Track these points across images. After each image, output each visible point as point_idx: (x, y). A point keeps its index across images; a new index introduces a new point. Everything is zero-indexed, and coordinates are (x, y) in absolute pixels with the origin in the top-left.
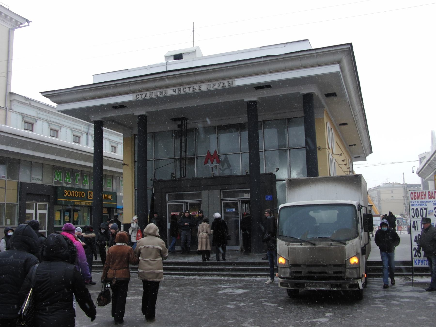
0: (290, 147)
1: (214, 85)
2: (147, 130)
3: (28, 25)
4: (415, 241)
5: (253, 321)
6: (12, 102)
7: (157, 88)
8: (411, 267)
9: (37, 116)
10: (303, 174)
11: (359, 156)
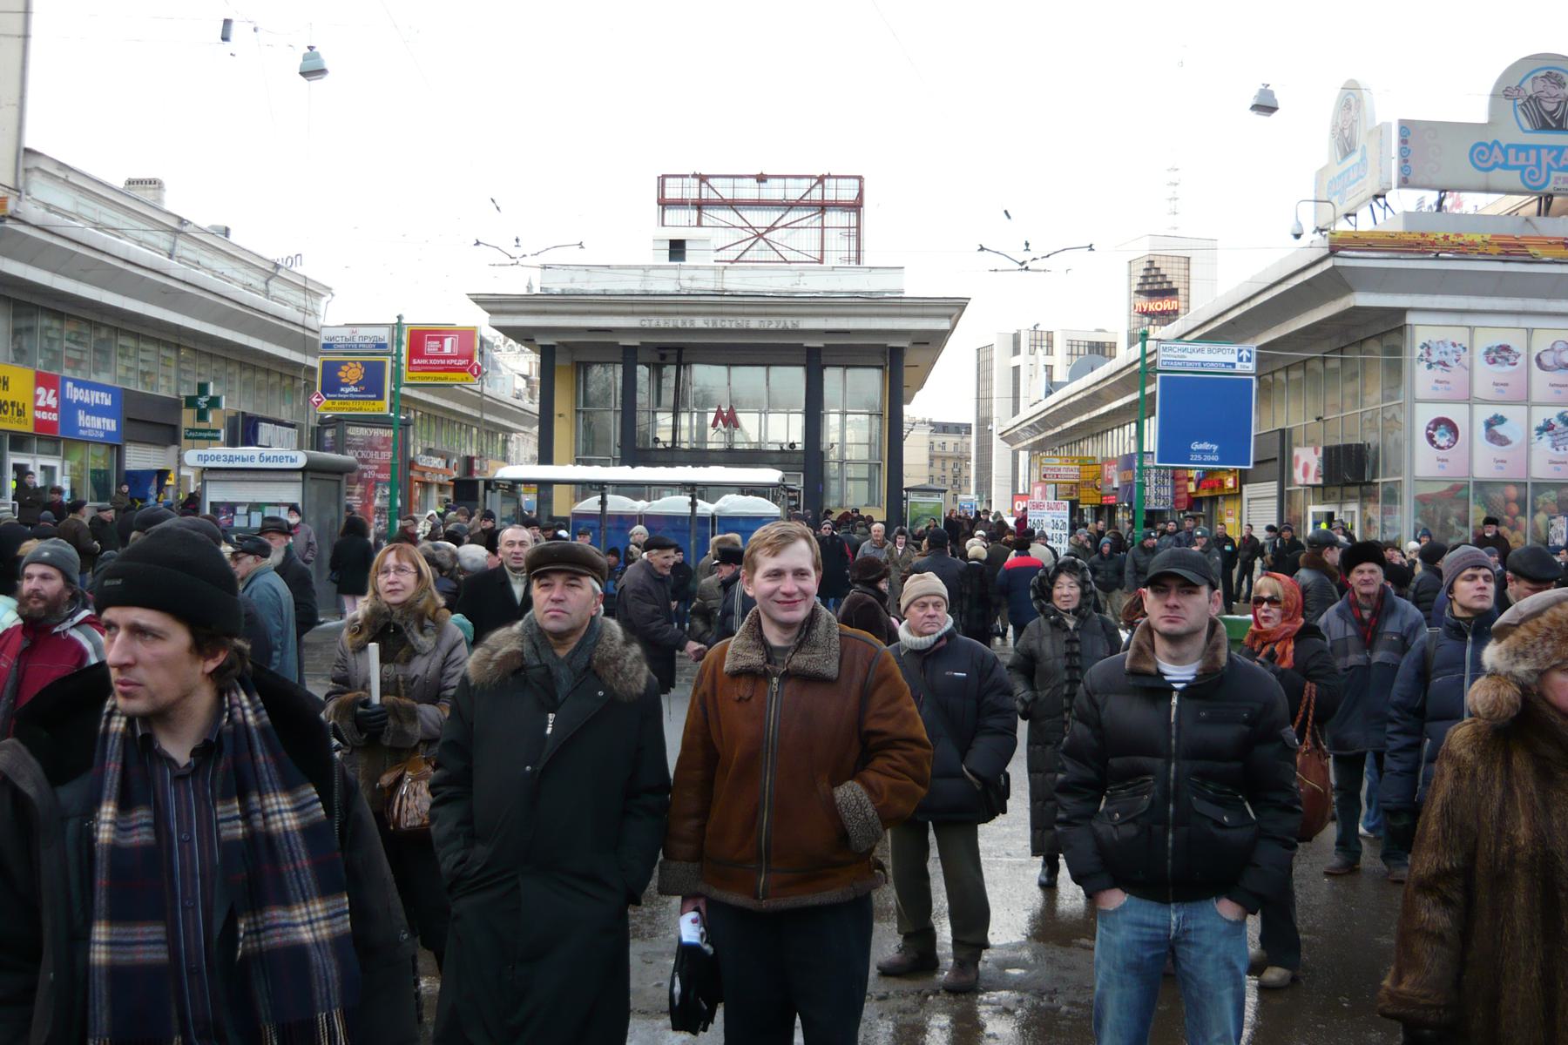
0: (334, 485)
1: (770, 323)
5: (1024, 718)
6: (29, 175)
9: (74, 211)
10: (1483, 705)
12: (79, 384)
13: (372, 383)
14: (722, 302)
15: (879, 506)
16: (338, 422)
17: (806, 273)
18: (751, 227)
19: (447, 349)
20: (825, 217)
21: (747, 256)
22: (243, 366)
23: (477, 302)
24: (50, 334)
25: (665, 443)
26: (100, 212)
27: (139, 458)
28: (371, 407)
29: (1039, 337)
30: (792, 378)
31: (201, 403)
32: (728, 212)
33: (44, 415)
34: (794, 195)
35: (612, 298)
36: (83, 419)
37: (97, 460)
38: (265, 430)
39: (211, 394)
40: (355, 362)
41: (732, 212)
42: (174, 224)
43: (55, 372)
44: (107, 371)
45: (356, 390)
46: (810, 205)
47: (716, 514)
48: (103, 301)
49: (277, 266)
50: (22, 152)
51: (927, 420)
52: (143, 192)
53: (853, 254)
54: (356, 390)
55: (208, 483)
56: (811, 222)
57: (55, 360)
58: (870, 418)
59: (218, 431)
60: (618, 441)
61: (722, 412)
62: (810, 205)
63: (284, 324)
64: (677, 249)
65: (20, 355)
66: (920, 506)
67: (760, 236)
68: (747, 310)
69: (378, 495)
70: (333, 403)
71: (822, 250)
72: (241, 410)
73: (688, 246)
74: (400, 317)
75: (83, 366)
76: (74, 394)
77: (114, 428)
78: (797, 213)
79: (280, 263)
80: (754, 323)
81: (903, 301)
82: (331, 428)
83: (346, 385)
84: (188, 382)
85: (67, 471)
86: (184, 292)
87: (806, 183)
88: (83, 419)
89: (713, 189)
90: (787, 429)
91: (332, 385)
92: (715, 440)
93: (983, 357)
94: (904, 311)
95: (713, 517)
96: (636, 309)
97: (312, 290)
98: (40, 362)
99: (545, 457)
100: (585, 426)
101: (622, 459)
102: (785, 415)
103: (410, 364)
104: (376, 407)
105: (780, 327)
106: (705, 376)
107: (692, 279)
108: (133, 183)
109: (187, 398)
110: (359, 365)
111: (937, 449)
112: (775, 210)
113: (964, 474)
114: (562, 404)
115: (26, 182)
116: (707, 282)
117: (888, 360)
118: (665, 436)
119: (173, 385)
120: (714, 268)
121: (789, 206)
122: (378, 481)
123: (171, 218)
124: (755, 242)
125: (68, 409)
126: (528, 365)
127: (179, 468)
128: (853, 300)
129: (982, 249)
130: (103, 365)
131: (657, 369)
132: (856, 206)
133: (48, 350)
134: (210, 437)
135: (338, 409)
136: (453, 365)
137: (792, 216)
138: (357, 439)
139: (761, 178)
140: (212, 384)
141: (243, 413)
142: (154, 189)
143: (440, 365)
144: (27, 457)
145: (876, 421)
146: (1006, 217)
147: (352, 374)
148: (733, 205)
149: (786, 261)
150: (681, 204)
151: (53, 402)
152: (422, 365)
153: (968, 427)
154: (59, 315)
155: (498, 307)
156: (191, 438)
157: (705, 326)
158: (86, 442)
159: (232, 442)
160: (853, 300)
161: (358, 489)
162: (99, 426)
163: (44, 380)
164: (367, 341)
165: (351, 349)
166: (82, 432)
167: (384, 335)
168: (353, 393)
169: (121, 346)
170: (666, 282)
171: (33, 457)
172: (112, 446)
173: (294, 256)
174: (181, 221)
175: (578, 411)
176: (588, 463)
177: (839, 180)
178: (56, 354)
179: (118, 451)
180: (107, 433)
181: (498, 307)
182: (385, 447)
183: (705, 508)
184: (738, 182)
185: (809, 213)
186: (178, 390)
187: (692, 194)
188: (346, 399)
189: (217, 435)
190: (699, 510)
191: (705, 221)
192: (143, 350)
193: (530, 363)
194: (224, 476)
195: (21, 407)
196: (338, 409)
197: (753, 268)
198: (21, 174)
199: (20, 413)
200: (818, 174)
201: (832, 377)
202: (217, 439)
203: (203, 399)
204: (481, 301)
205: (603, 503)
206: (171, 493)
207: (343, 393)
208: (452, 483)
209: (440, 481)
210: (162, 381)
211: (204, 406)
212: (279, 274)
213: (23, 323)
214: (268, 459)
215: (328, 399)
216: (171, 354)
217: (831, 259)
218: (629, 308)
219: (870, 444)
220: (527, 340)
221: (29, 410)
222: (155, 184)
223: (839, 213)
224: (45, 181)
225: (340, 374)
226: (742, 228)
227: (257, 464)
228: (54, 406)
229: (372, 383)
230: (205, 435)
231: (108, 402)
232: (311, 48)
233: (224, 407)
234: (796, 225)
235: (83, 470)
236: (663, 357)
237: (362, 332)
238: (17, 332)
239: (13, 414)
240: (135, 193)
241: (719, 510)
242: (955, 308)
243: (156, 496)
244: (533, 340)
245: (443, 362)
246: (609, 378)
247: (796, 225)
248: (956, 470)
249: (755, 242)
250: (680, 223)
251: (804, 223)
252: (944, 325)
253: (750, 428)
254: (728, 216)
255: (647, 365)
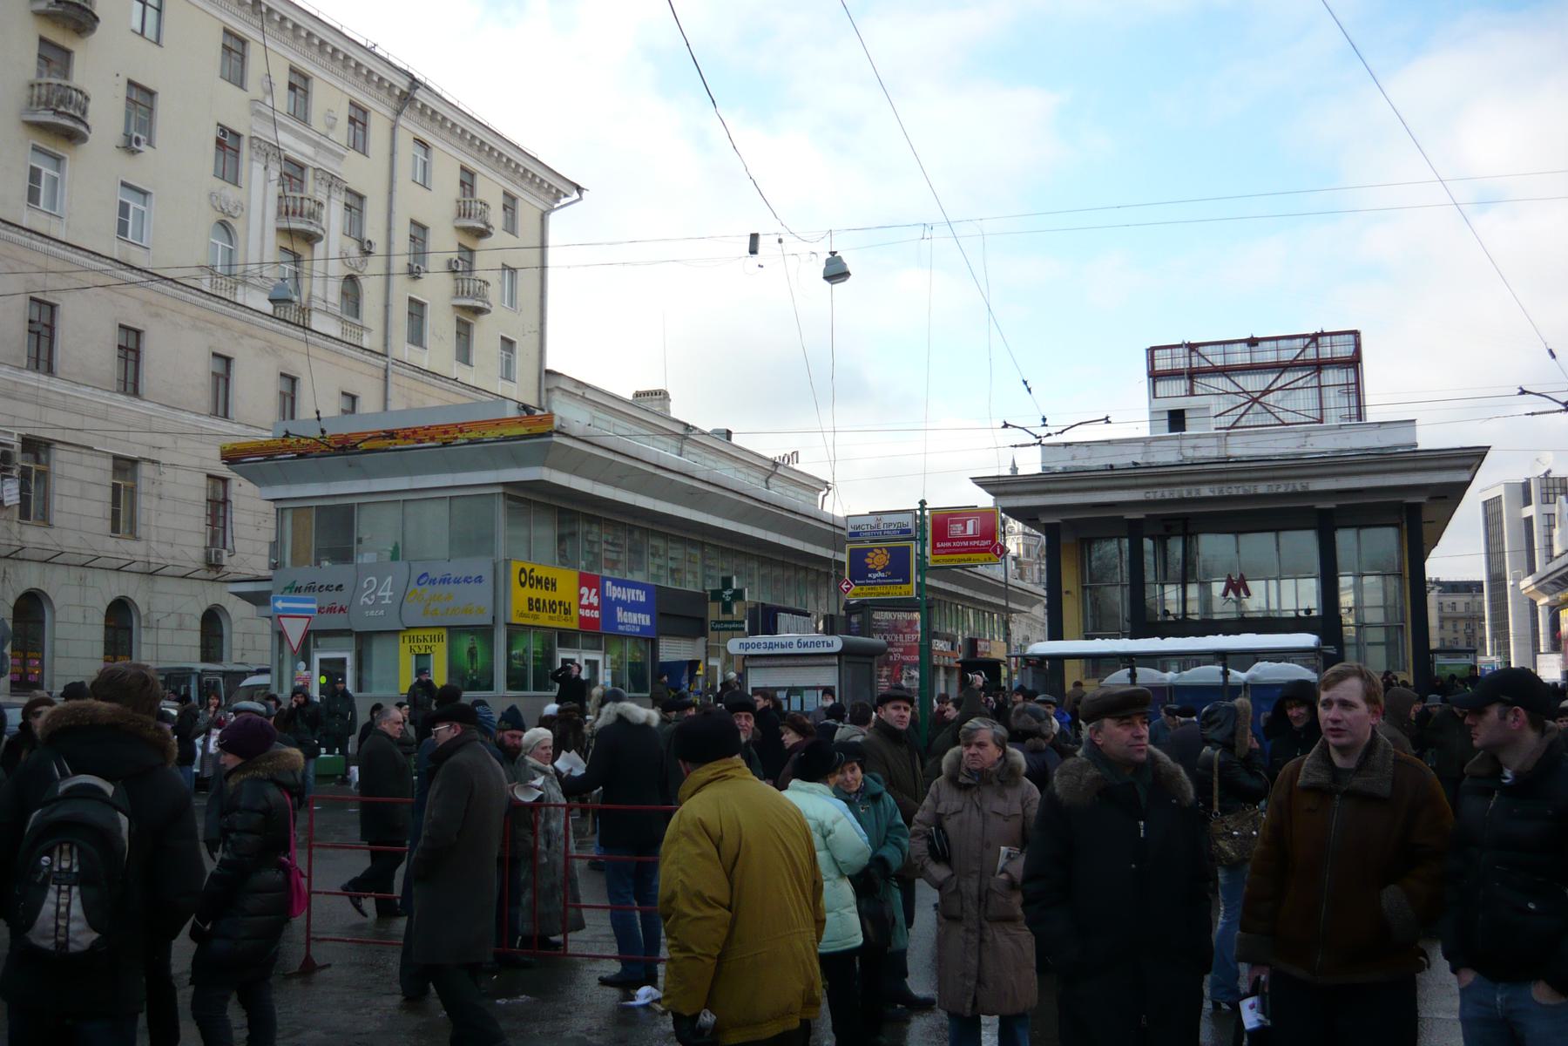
1: (1279, 487)
2: (1431, 644)
3: (581, 199)
4: (844, 609)
6: (550, 394)
7: (1182, 484)
8: (407, 853)
11: (1219, 431)
12: (616, 583)
13: (898, 567)
14: (1226, 469)
15: (1404, 670)
16: (863, 607)
17: (1313, 433)
18: (1245, 392)
19: (970, 531)
20: (1322, 375)
21: (1243, 422)
22: (764, 561)
23: (977, 483)
24: (590, 537)
25: (1175, 616)
26: (614, 424)
27: (673, 650)
28: (898, 591)
29: (1551, 484)
30: (1305, 542)
31: (725, 596)
32: (1220, 379)
33: (587, 613)
34: (1287, 356)
35: (1160, 470)
36: (622, 616)
37: (630, 652)
38: (784, 618)
39: (735, 587)
40: (880, 548)
41: (1224, 379)
42: (680, 430)
43: (596, 573)
44: (640, 570)
45: (883, 575)
46: (1305, 365)
47: (1250, 682)
48: (637, 505)
49: (775, 464)
50: (544, 373)
51: (1433, 579)
52: (649, 403)
53: (1354, 411)
54: (883, 575)
55: (749, 670)
56: (1307, 382)
57: (596, 560)
58: (1385, 581)
59: (743, 623)
60: (1126, 615)
61: (1233, 581)
62: (1305, 365)
63: (798, 518)
64: (1177, 419)
65: (565, 560)
66: (1448, 668)
67: (1255, 400)
68: (1276, 474)
69: (904, 676)
70: (862, 589)
71: (1321, 409)
72: (760, 602)
73: (1187, 415)
74: (923, 503)
75: (620, 566)
76: (614, 592)
77: (648, 623)
78: (1291, 374)
79: (777, 460)
80: (1262, 488)
81: (1418, 454)
82: (858, 613)
83: (875, 571)
84: (710, 577)
85: (608, 665)
86: (708, 492)
87: (1299, 343)
88: (622, 616)
89: (1203, 356)
90: (1302, 595)
91: (860, 571)
92: (1222, 608)
93: (1491, 510)
94: (1419, 465)
95: (1246, 684)
96: (1140, 481)
97: (818, 486)
98: (583, 563)
99: (1056, 633)
100: (1092, 603)
101: (1131, 633)
102: (1293, 581)
103: (934, 547)
104: (902, 591)
105: (1289, 490)
106: (1214, 547)
107: (1194, 447)
108: (640, 396)
109: (712, 591)
110: (885, 551)
111: (1447, 610)
112: (1268, 373)
113: (1478, 634)
114: (1069, 582)
115: (549, 401)
116: (1210, 451)
117: (1405, 517)
118: (1174, 608)
119: (699, 580)
120: (1216, 436)
121: (1280, 367)
122: (904, 663)
123: (677, 424)
124: (1250, 407)
125: (607, 606)
126: (1016, 546)
127: (707, 659)
128: (1365, 458)
129: (1006, 426)
130: (636, 563)
131: (1161, 541)
132: (1353, 362)
133: (588, 552)
134: (735, 628)
135: (866, 594)
136: (976, 546)
137: (1287, 377)
138: (883, 624)
139: (1253, 342)
140: (734, 578)
141: (763, 604)
142: (660, 399)
143: (963, 547)
144: (573, 652)
145: (1393, 583)
146: (1549, 357)
147: (878, 560)
148: (1225, 371)
149: (1284, 424)
150: (1173, 374)
151: (595, 601)
152: (946, 548)
153: (1480, 584)
154: (592, 519)
155: (1002, 489)
156: (717, 630)
157: (1211, 494)
158: (623, 637)
159: (754, 631)
160: (1365, 458)
161: (885, 672)
162: (635, 621)
163: (587, 580)
164: (892, 528)
165: (877, 536)
166: (621, 628)
167: (908, 521)
168: (881, 578)
169: (653, 547)
170: (1166, 455)
171: (578, 653)
172: (646, 640)
173: (790, 454)
174: (687, 426)
175: (1084, 588)
176: (1092, 638)
177: (1334, 337)
178: (597, 556)
179: (654, 645)
180: (642, 627)
181: (1002, 489)
182: (909, 630)
183: (1237, 676)
184: (1229, 348)
185: (1304, 374)
186: (704, 585)
187: (1181, 363)
188: (875, 584)
189: (742, 626)
190: (1231, 679)
191: (1198, 390)
192: (671, 548)
193: (1018, 544)
194: (764, 662)
195: (567, 606)
196: (866, 594)
197: (1257, 433)
198: (544, 393)
199: (567, 611)
200: (1311, 331)
201: (1345, 539)
202: (743, 629)
203: (728, 592)
204: (984, 483)
205: (1133, 676)
206: (700, 682)
207: (871, 579)
208: (959, 665)
209: (947, 664)
210: (689, 577)
211: (728, 599)
212: (778, 471)
213: (566, 531)
214: (806, 645)
215: (856, 585)
216: (697, 553)
217: (1332, 419)
218: (1133, 482)
219: (1385, 607)
220: (1030, 520)
221: (574, 608)
222: (662, 395)
223: (1336, 371)
224: (565, 400)
225: (867, 561)
226: (1236, 393)
227: (795, 650)
228: (596, 604)
229: (898, 567)
230: (730, 626)
231: (642, 599)
232: (833, 253)
233: (747, 599)
234: (1292, 386)
235: (622, 663)
236: (1168, 528)
237: (887, 519)
238: (561, 539)
239: (560, 613)
240: (643, 405)
241: (1252, 678)
242: (1473, 457)
243: (687, 686)
244: (1037, 519)
245: (966, 544)
246: (1113, 551)
247: (1292, 386)
248: (1468, 631)
249: (1250, 407)
250: (1174, 394)
251: (1300, 383)
252: (1462, 476)
253: (1259, 598)
254: (1220, 383)
255: (1151, 537)
